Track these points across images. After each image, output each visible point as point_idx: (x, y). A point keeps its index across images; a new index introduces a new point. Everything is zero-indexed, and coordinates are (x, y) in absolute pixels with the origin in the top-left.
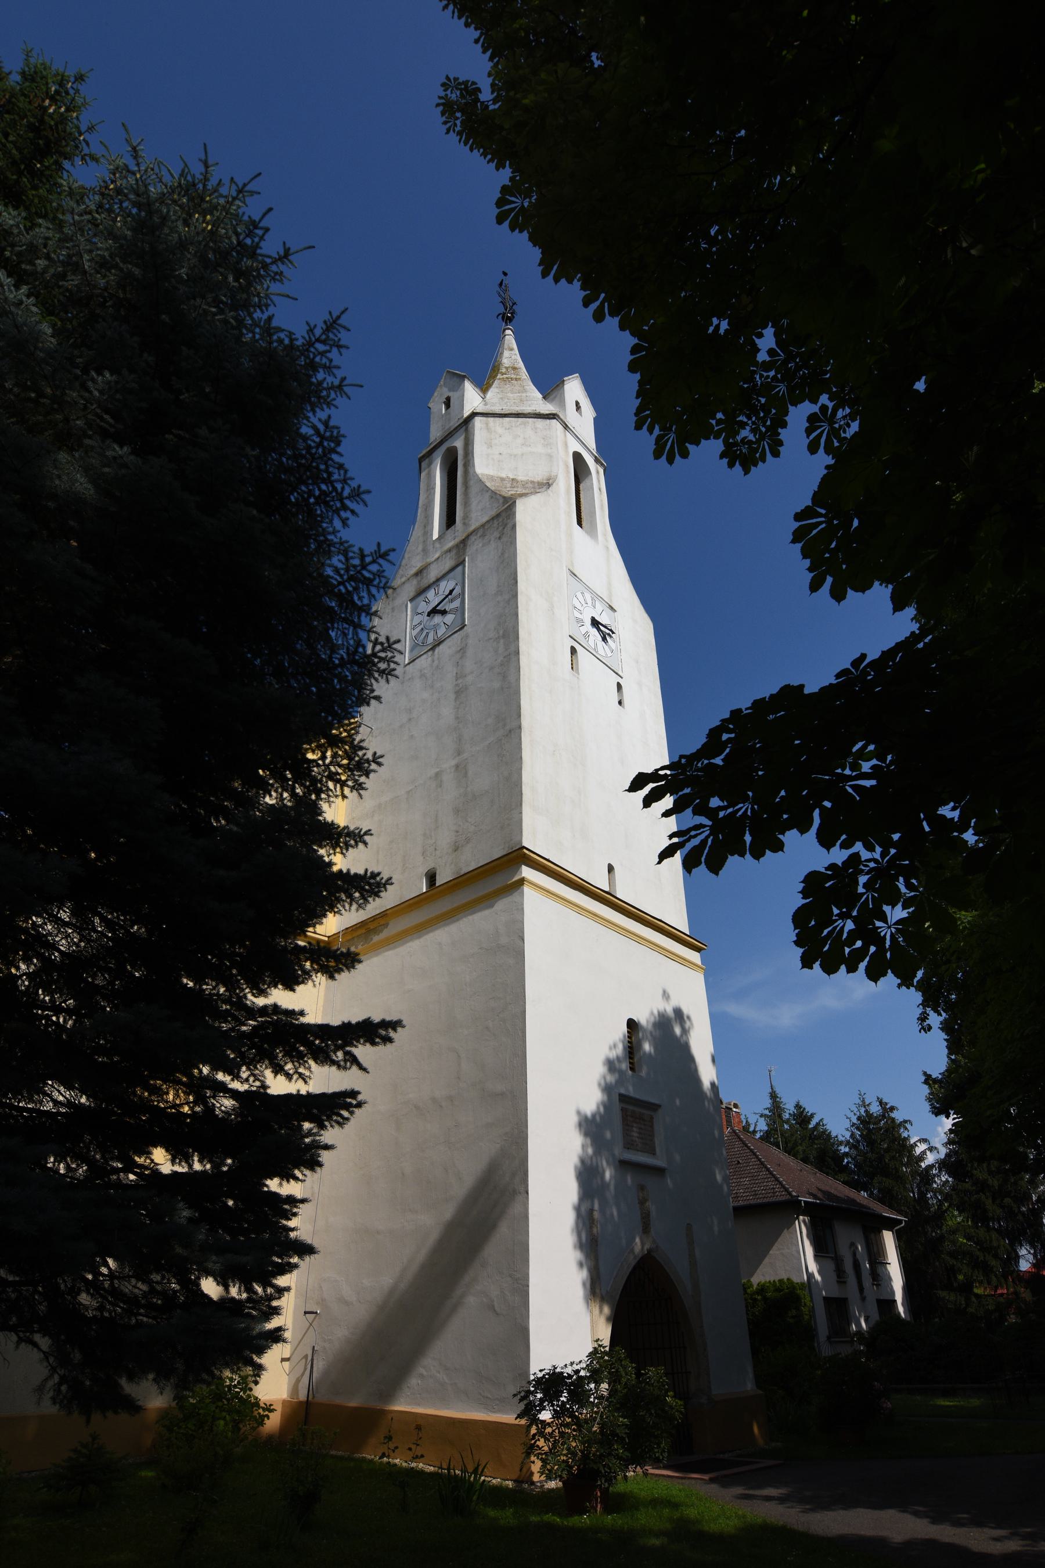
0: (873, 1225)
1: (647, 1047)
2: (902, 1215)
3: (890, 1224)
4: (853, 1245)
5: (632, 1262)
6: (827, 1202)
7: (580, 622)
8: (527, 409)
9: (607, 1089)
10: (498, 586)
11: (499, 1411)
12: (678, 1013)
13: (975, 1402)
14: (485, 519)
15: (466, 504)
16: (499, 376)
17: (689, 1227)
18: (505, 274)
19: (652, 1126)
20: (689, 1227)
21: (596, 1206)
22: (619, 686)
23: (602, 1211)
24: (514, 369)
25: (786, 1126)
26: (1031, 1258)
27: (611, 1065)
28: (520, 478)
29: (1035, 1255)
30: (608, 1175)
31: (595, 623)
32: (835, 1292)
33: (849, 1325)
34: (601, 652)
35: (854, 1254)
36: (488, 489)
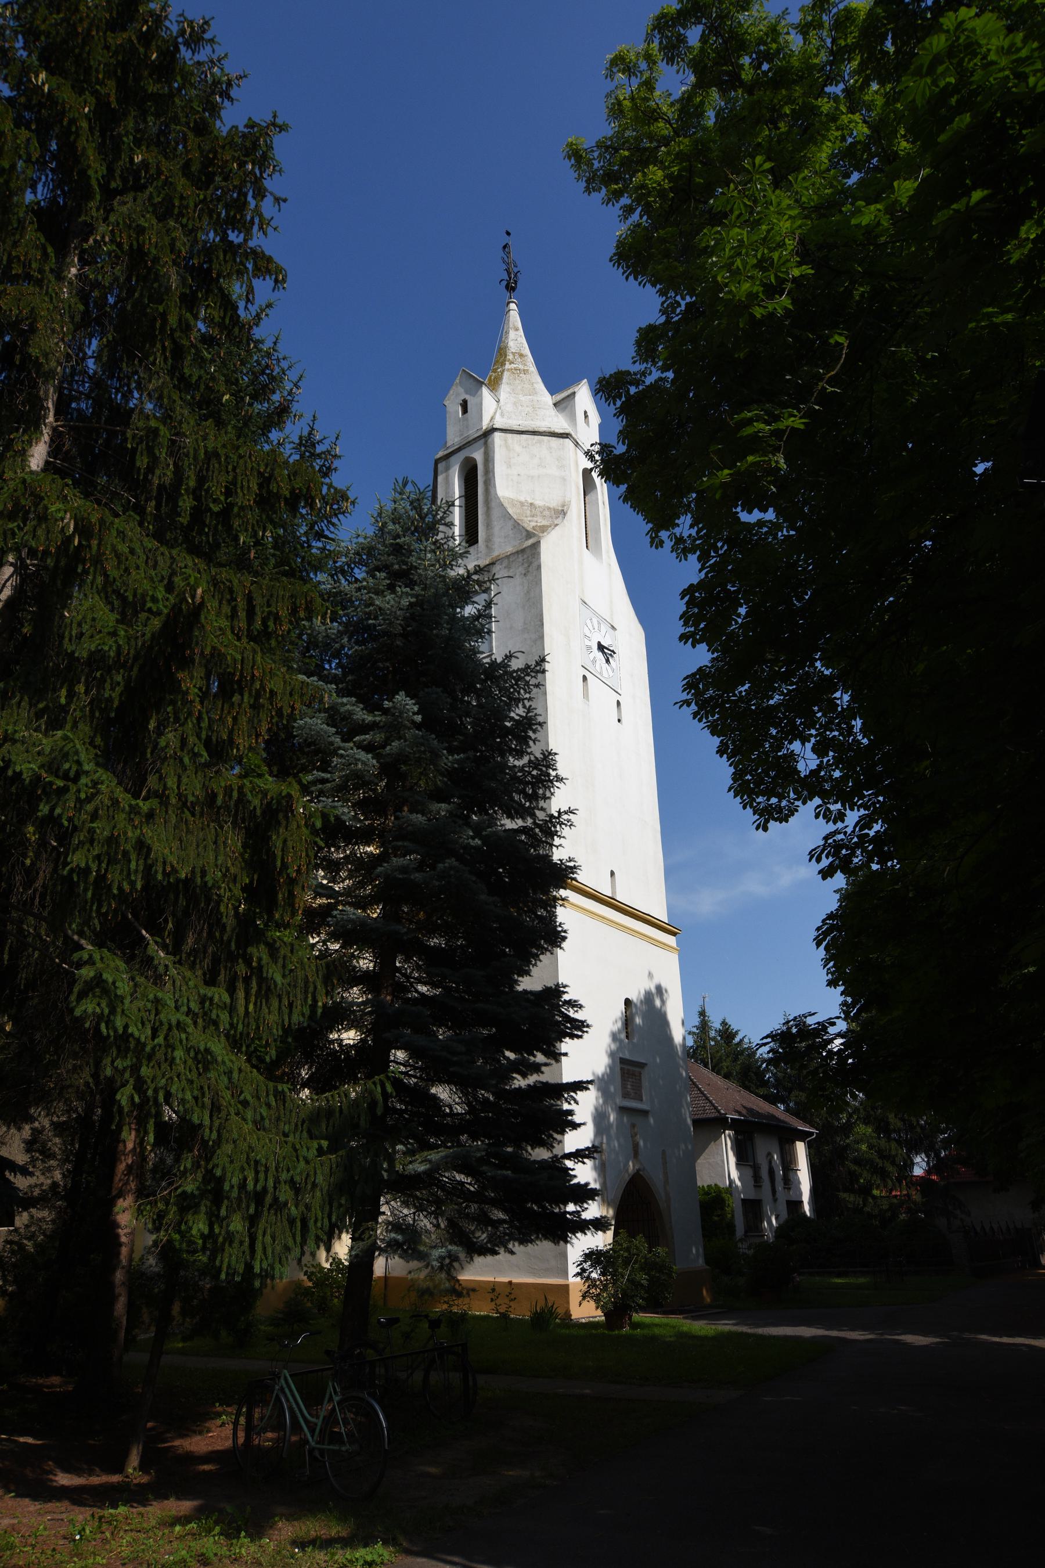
0: (787, 1137)
1: (638, 1020)
2: (813, 1126)
3: (802, 1136)
4: (769, 1155)
5: (627, 1178)
6: (750, 1118)
7: (589, 648)
8: (542, 425)
9: (612, 1055)
10: (525, 623)
11: (544, 1277)
12: (659, 988)
13: (862, 1280)
14: (510, 549)
15: (488, 526)
16: (507, 366)
17: (664, 1152)
18: (508, 234)
19: (640, 1080)
20: (664, 1152)
21: (605, 1141)
22: (618, 703)
23: (608, 1144)
24: (521, 355)
25: (712, 1043)
26: (924, 1165)
27: (614, 1037)
28: (538, 503)
29: (928, 1163)
30: (612, 1118)
31: (601, 647)
32: (752, 1195)
33: (762, 1222)
34: (605, 674)
35: (770, 1162)
36: (511, 517)
